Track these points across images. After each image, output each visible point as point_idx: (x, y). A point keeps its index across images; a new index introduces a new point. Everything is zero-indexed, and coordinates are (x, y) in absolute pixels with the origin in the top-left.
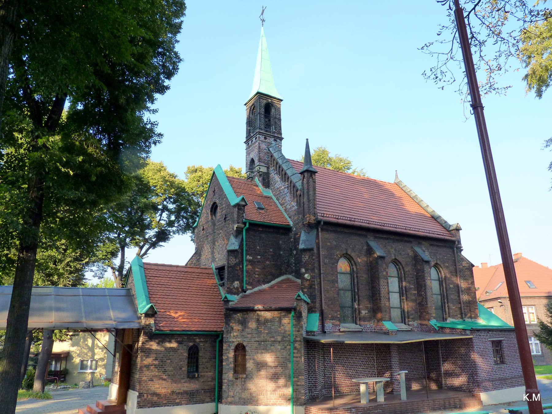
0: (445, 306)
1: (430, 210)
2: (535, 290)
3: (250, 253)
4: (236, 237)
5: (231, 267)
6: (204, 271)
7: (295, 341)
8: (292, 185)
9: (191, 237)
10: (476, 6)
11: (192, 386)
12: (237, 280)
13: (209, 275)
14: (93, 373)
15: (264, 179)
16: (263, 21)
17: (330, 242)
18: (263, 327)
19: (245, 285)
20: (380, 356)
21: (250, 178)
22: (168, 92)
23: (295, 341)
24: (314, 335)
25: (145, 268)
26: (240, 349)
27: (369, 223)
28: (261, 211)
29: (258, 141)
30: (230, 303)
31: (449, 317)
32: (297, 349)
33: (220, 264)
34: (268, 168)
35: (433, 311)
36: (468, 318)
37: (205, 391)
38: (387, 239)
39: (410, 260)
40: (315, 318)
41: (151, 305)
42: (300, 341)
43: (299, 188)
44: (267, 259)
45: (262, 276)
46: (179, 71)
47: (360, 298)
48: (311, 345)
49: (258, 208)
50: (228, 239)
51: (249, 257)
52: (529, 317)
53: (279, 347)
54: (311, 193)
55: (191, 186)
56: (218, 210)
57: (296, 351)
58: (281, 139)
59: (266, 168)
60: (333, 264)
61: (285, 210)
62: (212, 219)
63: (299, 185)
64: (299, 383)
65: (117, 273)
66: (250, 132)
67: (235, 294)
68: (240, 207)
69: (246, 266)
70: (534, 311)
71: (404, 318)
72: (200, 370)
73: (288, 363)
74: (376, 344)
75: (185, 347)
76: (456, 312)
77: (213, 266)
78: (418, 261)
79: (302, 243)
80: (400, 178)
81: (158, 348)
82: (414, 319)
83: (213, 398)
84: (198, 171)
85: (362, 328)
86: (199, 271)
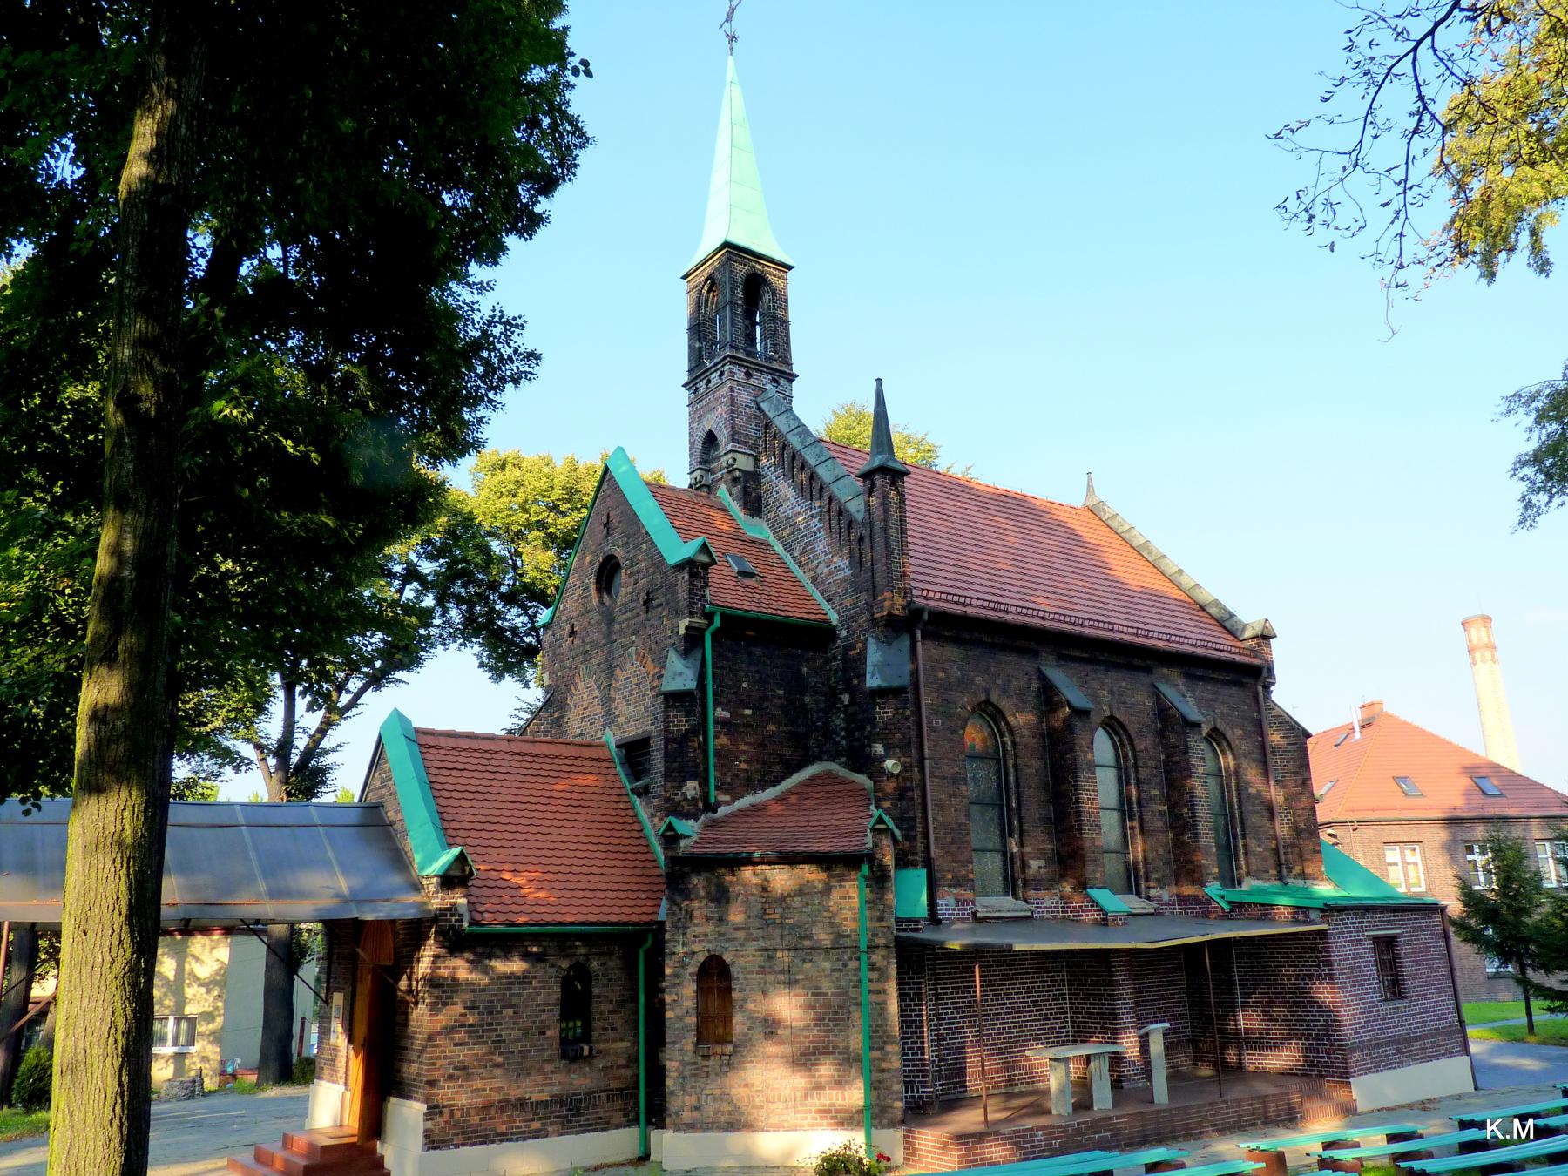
0: (1236, 847)
1: (1186, 582)
2: (1420, 802)
3: (723, 700)
4: (686, 654)
5: (675, 740)
6: (587, 753)
7: (872, 947)
8: (835, 508)
9: (479, 656)
10: (1437, 24)
11: (581, 1080)
12: (693, 777)
13: (600, 763)
14: (179, 1057)
15: (746, 492)
16: (732, 38)
17: (944, 670)
18: (779, 910)
19: (713, 792)
20: (1085, 988)
21: (702, 487)
22: (542, 231)
23: (872, 947)
24: (916, 930)
25: (421, 745)
26: (715, 976)
27: (1043, 618)
28: (748, 582)
29: (729, 383)
30: (683, 843)
31: (1248, 874)
32: (878, 969)
33: (633, 732)
34: (757, 460)
35: (1209, 861)
36: (1296, 877)
37: (611, 1095)
38: (1089, 661)
39: (1148, 721)
40: (916, 879)
41: (457, 850)
42: (887, 947)
43: (860, 517)
44: (771, 718)
45: (758, 766)
46: (578, 171)
47: (1026, 826)
48: (917, 958)
49: (740, 573)
50: (661, 662)
51: (723, 713)
52: (1406, 875)
53: (827, 965)
54: (894, 532)
55: (492, 509)
56: (623, 576)
57: (875, 975)
58: (791, 377)
59: (751, 460)
60: (954, 731)
61: (814, 580)
62: (601, 603)
63: (856, 507)
64: (884, 1065)
65: (272, 761)
66: (700, 357)
67: (687, 816)
68: (696, 569)
69: (716, 737)
70: (1418, 859)
71: (1132, 882)
72: (595, 1035)
73: (853, 1008)
74: (1068, 951)
75: (552, 971)
76: (1265, 860)
77: (610, 738)
78: (1169, 722)
79: (873, 674)
80: (1101, 493)
81: (474, 977)
82: (1161, 883)
83: (632, 1115)
84: (509, 466)
85: (1033, 907)
86: (572, 751)
